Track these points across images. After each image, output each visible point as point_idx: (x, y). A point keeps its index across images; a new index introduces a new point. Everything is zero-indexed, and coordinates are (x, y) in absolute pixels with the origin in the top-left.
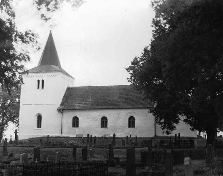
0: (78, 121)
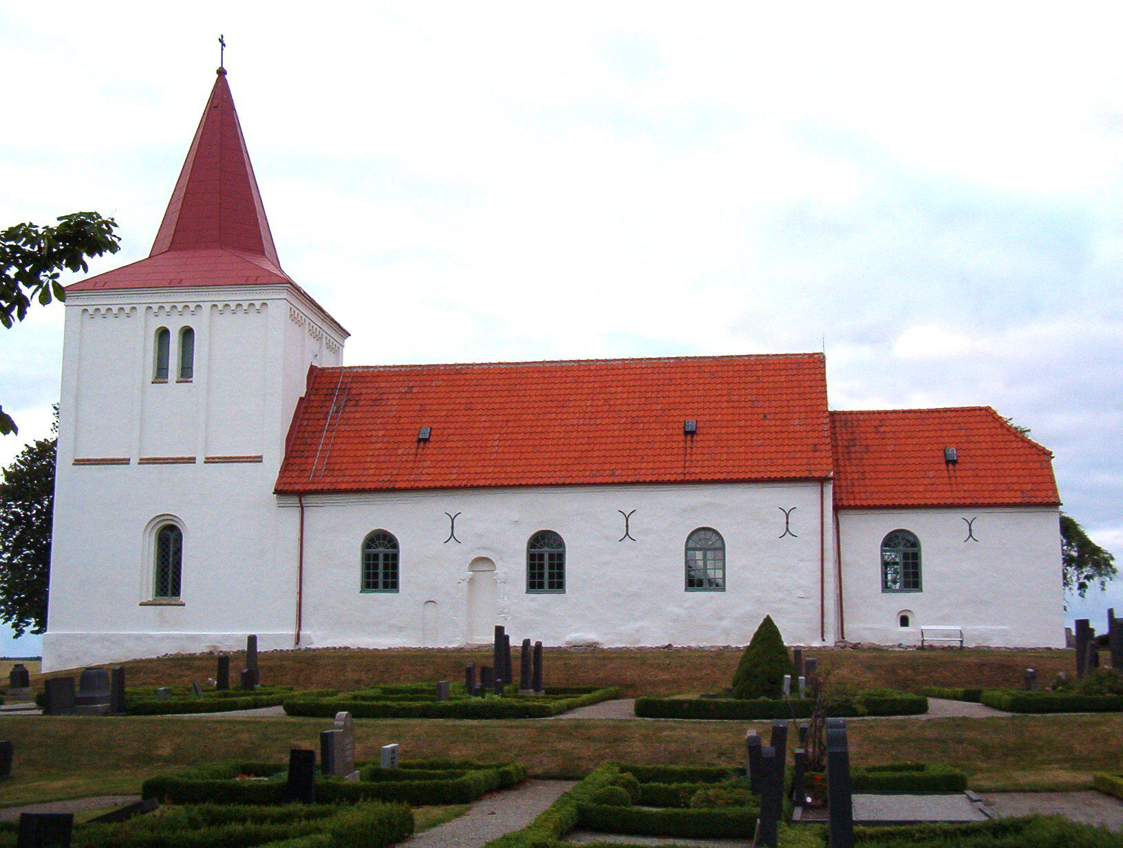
0: (395, 557)
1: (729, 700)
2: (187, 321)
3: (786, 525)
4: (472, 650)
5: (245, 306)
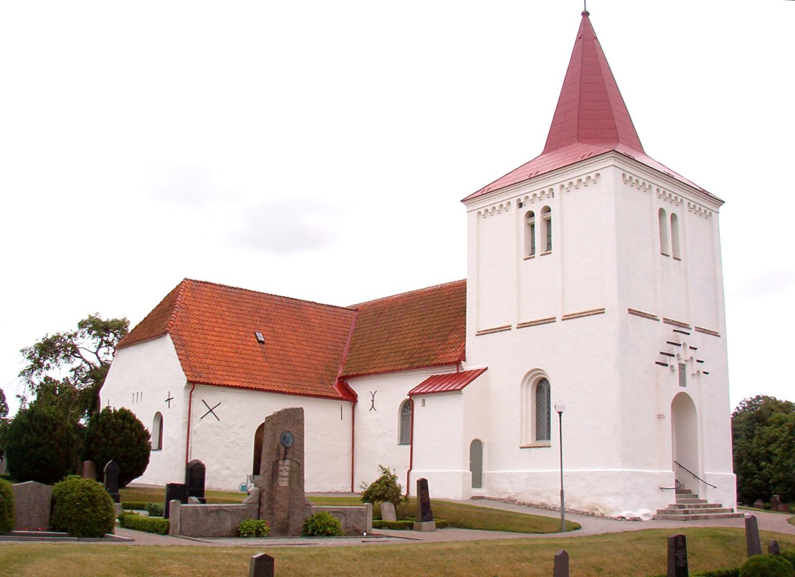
1: (754, 563)
2: (546, 202)
5: (584, 180)
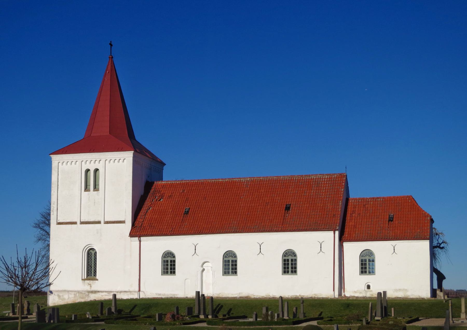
2: (97, 166)
3: (195, 250)
4: (353, 300)
